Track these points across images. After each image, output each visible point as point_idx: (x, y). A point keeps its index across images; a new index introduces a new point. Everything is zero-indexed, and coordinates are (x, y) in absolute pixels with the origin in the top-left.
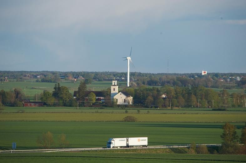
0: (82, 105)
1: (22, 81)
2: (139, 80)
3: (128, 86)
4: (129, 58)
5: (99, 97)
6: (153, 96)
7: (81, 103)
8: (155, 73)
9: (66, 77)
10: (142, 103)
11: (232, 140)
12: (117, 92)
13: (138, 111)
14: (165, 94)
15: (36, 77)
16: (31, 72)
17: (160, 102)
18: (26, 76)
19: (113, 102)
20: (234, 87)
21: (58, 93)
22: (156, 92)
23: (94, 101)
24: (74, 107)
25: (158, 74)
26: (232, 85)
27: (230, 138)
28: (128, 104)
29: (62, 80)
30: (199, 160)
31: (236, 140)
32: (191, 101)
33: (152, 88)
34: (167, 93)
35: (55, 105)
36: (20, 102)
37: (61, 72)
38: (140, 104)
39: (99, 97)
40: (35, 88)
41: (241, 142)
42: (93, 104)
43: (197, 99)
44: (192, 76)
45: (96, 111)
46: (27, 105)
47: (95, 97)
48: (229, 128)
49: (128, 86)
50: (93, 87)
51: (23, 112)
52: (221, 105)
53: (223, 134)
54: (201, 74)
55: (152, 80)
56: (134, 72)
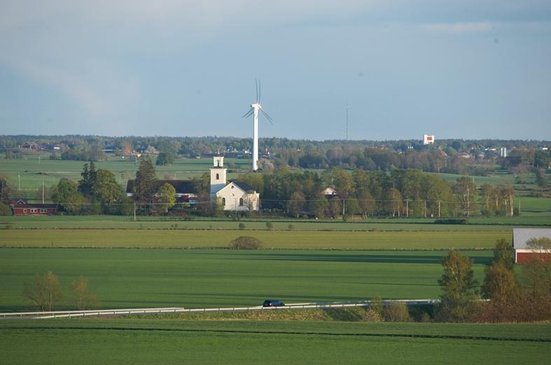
0: (144, 211)
1: (17, 157)
2: (281, 156)
3: (256, 168)
4: (257, 107)
5: (186, 194)
6: (305, 192)
7: (143, 207)
8: (319, 140)
9: (117, 148)
10: (280, 207)
11: (464, 289)
12: (225, 182)
13: (268, 225)
14: (332, 188)
15: (50, 148)
16: (41, 137)
17: (321, 205)
18: (28, 146)
19: (215, 206)
20: (492, 171)
21: (90, 184)
22: (311, 183)
23: (173, 203)
24: (126, 215)
25: (326, 142)
26: (489, 166)
27: (458, 286)
28: (248, 209)
29: (109, 155)
30: (383, 335)
31: (472, 291)
32: (390, 202)
33: (303, 173)
34: (337, 184)
35: (83, 212)
36: (5, 206)
37: (110, 138)
38: (275, 210)
39: (186, 194)
40: (45, 174)
41: (484, 294)
42: (169, 210)
43: (404, 197)
44: (402, 146)
45: (172, 226)
46: (21, 212)
47: (174, 194)
48: (457, 264)
49: (256, 168)
50: (179, 171)
51: (7, 228)
52: (457, 210)
53: (444, 276)
54: (422, 142)
55: (309, 157)
56: (272, 137)
